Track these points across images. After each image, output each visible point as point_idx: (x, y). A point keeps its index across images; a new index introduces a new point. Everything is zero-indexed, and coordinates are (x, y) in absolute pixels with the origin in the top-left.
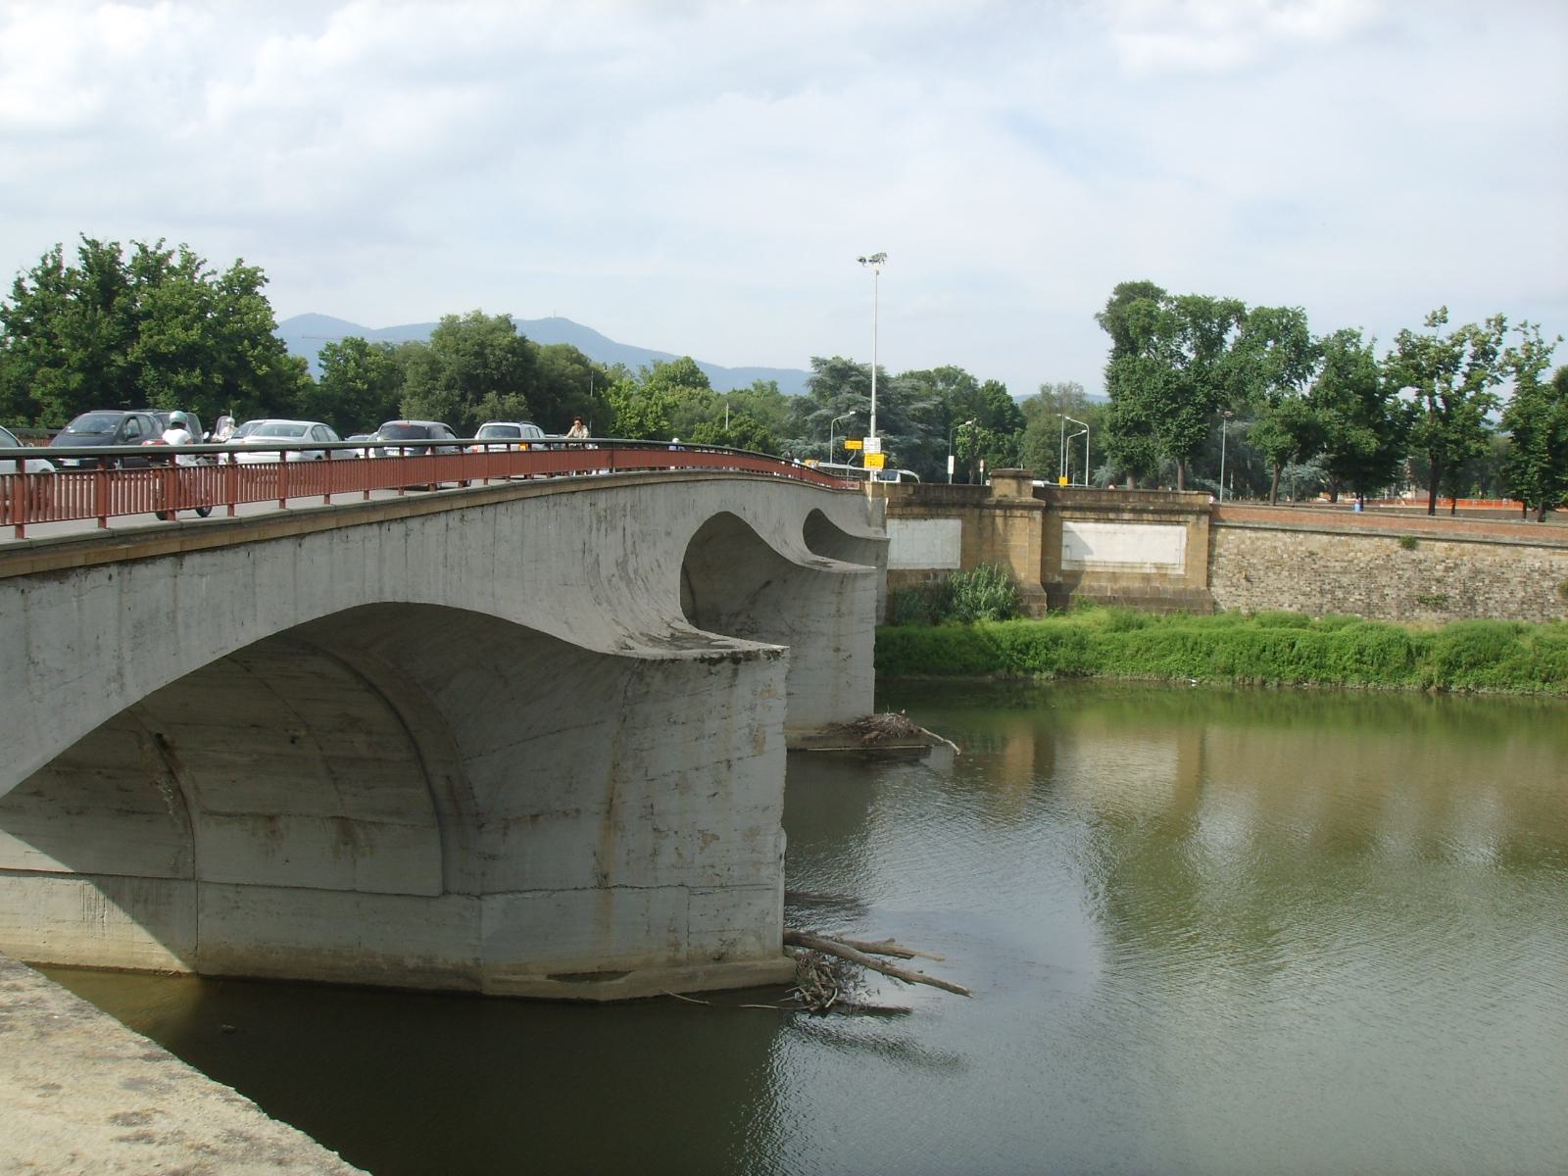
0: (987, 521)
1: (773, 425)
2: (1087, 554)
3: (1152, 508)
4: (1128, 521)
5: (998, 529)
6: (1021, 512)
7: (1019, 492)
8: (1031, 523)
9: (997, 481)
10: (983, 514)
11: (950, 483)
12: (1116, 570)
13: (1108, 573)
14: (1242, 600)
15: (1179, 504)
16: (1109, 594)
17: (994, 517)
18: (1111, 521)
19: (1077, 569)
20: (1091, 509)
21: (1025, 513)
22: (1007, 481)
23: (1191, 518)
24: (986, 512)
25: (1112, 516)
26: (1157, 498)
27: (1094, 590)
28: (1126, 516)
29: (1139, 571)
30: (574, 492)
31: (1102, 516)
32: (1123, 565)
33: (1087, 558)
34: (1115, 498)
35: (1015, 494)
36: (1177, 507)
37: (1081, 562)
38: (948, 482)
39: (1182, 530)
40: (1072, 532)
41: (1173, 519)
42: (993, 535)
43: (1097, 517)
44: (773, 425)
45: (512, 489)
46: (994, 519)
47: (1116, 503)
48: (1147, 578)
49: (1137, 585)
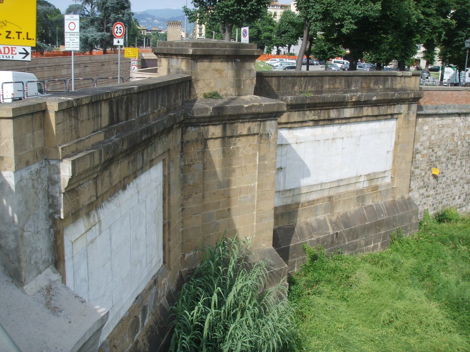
0: (194, 150)
1: (424, 319)
2: (304, 177)
3: (375, 98)
4: (347, 120)
5: (212, 163)
6: (247, 125)
7: (238, 85)
8: (264, 145)
9: (202, 65)
10: (187, 138)
11: (73, 90)
12: (332, 193)
13: (323, 199)
14: (430, 201)
15: (395, 90)
16: (331, 232)
17: (204, 141)
18: (330, 121)
19: (289, 202)
20: (313, 106)
21: (254, 126)
22: (218, 65)
23: (403, 108)
24: (192, 132)
25: (333, 114)
26: (376, 83)
27: (314, 230)
28: (348, 112)
29: (351, 188)
30: (90, 137)
31: (323, 115)
32: (339, 183)
33: (305, 182)
34: (337, 86)
35: (231, 92)
36: (397, 95)
37: (295, 191)
38: (72, 89)
39: (391, 125)
40: (287, 145)
41: (389, 111)
42: (203, 178)
43: (317, 118)
44: (424, 319)
45: (457, 115)
46: (206, 146)
47: (340, 94)
48: (361, 196)
49: (352, 208)
